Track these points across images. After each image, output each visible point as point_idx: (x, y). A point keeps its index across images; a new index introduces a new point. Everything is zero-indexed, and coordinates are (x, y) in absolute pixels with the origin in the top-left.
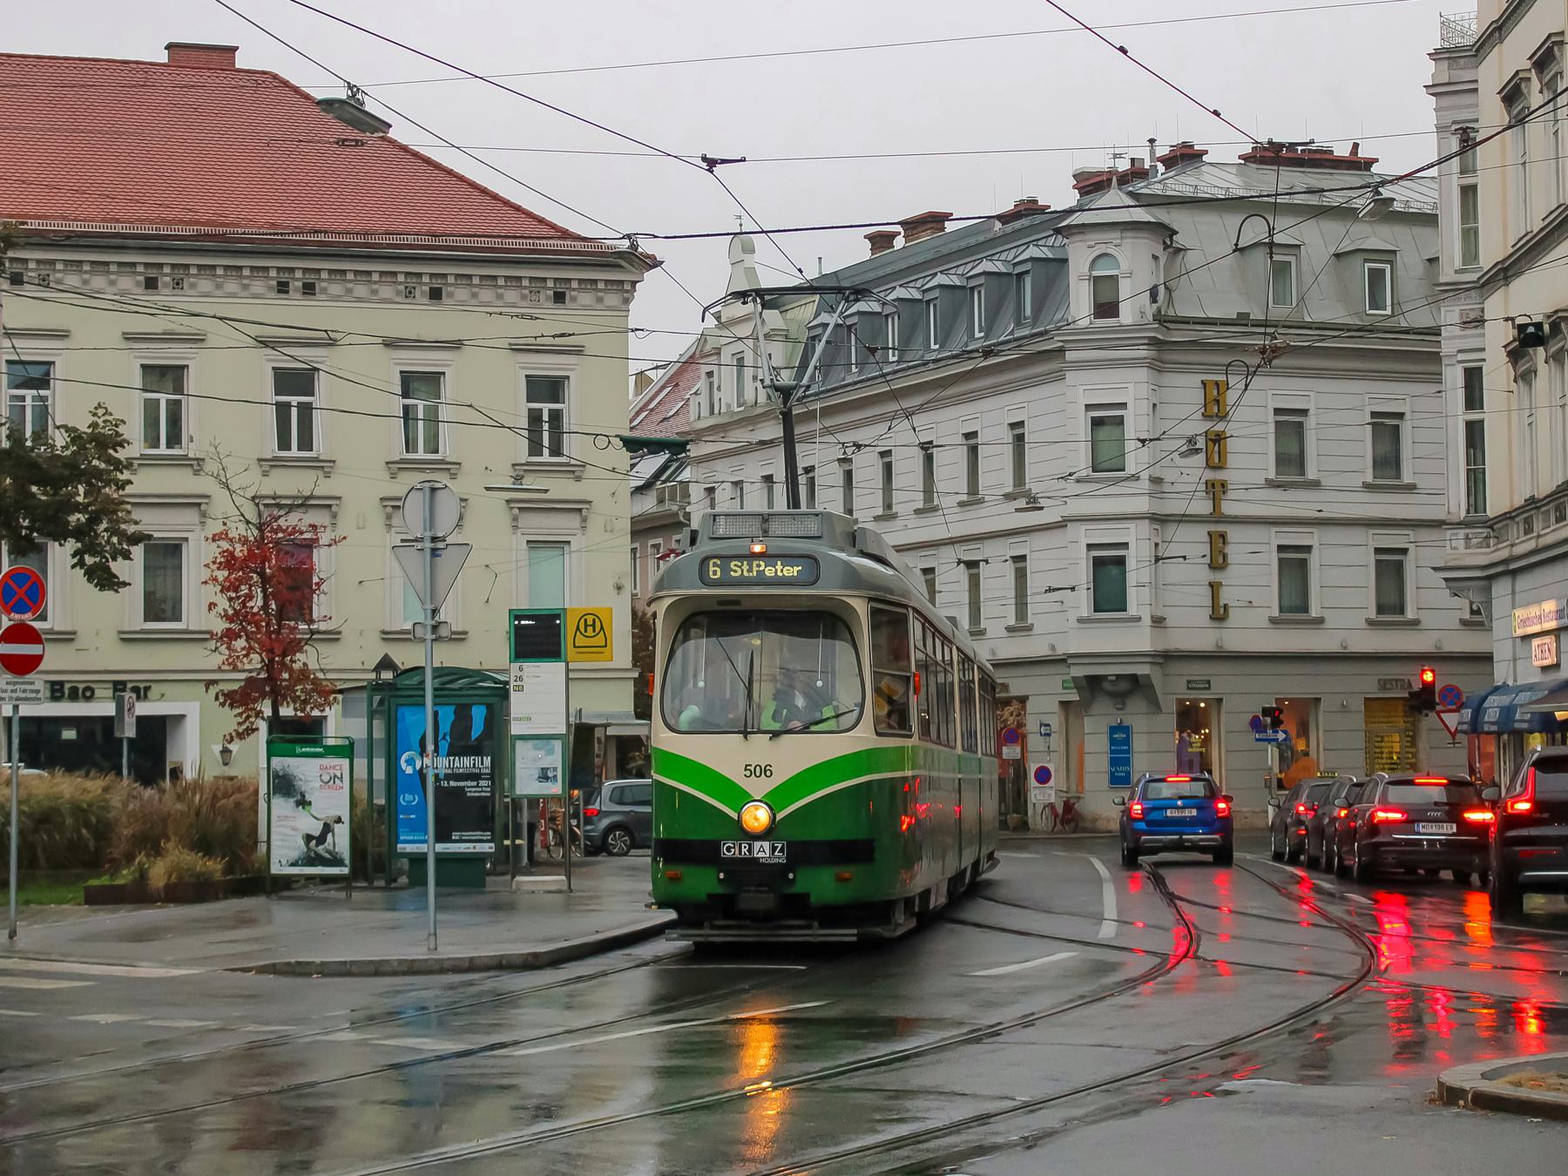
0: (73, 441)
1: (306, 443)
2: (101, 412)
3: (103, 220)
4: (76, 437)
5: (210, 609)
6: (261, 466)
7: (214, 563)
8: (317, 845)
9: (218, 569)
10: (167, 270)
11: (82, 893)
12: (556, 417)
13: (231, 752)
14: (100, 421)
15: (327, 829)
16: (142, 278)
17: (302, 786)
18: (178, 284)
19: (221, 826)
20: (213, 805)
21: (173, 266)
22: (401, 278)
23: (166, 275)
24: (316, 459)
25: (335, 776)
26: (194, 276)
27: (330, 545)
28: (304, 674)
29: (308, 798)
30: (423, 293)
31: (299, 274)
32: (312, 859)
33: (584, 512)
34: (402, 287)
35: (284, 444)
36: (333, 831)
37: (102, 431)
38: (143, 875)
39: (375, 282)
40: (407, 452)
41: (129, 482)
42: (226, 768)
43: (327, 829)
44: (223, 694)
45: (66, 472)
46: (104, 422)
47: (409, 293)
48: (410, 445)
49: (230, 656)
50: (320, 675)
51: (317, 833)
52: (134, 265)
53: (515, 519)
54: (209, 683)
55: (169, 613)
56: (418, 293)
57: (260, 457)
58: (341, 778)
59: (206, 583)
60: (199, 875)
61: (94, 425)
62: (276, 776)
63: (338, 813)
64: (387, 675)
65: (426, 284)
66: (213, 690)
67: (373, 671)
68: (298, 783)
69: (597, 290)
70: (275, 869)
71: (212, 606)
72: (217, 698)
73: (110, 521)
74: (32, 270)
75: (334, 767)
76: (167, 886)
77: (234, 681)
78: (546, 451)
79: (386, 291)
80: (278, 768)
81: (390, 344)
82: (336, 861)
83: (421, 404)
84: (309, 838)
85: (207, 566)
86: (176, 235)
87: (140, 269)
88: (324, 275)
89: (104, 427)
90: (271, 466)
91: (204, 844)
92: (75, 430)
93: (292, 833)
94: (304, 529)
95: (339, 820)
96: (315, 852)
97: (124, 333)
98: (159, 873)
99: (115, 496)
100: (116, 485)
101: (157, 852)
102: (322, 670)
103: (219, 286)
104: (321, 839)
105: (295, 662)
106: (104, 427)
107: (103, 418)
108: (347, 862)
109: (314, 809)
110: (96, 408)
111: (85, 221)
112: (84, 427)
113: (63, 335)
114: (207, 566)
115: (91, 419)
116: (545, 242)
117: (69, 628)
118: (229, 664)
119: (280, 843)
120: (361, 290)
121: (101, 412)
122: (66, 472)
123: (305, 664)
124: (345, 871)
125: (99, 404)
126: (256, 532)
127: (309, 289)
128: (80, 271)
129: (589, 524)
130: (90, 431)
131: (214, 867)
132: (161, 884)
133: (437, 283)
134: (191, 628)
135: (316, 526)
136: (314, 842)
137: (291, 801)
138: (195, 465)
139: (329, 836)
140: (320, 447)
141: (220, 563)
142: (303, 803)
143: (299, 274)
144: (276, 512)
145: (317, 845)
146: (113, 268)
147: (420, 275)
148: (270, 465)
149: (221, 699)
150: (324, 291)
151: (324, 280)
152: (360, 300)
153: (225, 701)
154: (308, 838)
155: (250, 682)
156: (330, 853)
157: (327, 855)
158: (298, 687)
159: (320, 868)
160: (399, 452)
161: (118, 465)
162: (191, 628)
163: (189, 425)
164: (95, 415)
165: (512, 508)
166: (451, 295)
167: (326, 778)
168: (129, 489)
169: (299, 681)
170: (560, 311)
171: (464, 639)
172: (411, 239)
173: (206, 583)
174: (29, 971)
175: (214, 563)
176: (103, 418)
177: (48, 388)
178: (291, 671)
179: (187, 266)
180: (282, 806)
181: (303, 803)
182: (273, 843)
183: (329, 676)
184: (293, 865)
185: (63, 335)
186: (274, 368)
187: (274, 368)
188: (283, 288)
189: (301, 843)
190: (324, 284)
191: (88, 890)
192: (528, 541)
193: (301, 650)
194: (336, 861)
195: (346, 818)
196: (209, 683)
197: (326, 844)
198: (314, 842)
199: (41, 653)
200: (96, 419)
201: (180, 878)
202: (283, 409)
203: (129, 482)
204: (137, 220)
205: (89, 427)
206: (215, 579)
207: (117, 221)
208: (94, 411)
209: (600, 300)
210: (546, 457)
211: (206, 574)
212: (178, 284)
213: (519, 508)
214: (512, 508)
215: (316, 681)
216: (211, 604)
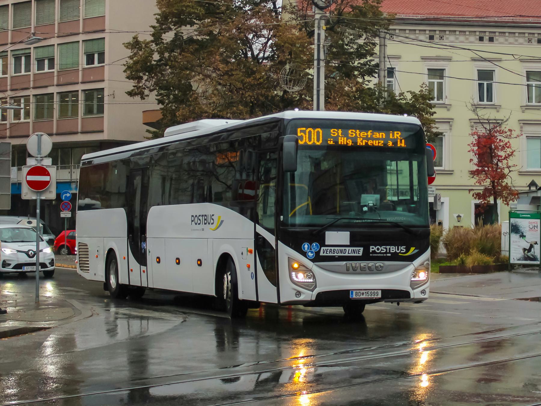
0: (413, 97)
1: (490, 99)
2: (424, 86)
3: (413, 14)
4: (414, 96)
5: (470, 162)
6: (522, 109)
7: (472, 144)
8: (528, 253)
9: (473, 146)
10: (437, 32)
11: (439, 268)
12: (440, 85)
13: (461, 217)
14: (424, 90)
15: (531, 246)
16: (478, 37)
17: (522, 229)
18: (441, 38)
19: (489, 245)
20: (486, 236)
21: (440, 31)
22: (527, 35)
23: (437, 34)
24: (494, 105)
25: (535, 226)
26: (448, 34)
27: (516, 137)
28: (506, 187)
29: (524, 234)
30: (535, 41)
31: (487, 34)
32: (527, 258)
33: (451, 123)
34: (527, 39)
35: (481, 99)
36: (534, 247)
37: (425, 93)
38: (463, 262)
39: (507, 36)
40: (529, 102)
41: (435, 113)
42: (459, 223)
43: (531, 246)
44: (476, 194)
45: (412, 109)
46: (425, 90)
47: (530, 41)
48: (529, 99)
49: (479, 180)
50: (513, 189)
51: (528, 248)
52: (425, 30)
53: (521, 127)
54: (470, 190)
55: (437, 164)
56: (533, 41)
57: (521, 105)
58: (537, 227)
59: (469, 151)
60: (485, 263)
61: (422, 91)
62: (512, 225)
63: (536, 240)
64: (533, 188)
65: (536, 37)
66: (472, 193)
67: (528, 186)
68: (521, 229)
69: (515, 37)
70: (512, 261)
71: (471, 160)
72: (473, 196)
73: (427, 127)
74: (437, 34)
75: (534, 223)
76: (473, 267)
77: (480, 189)
78: (436, 99)
79: (521, 40)
80: (513, 223)
81: (424, 59)
82: (534, 259)
83: (485, 83)
84: (525, 250)
85: (469, 145)
86: (412, 19)
87: (478, 33)
88: (497, 34)
89: (425, 92)
90: (526, 109)
91: (483, 251)
92: (414, 93)
93: (518, 247)
94: (507, 131)
95: (536, 243)
96: (527, 255)
97: (421, 57)
98: (470, 261)
99: (429, 117)
100: (430, 114)
101: (468, 253)
102: (514, 187)
103: (457, 39)
104: (529, 250)
105: (503, 182)
106: (425, 92)
107: (425, 88)
108: (539, 259)
109: (526, 239)
110: (422, 85)
111: (406, 14)
112: (417, 92)
113: (449, 59)
114: (469, 145)
115: (420, 89)
116: (508, 18)
117: (451, 169)
118: (479, 183)
119: (514, 251)
120: (511, 40)
121: (424, 86)
122: (412, 109)
123: (507, 183)
124: (538, 263)
125: (423, 83)
126: (488, 132)
127: (491, 40)
128: (505, 36)
129: (453, 128)
130: (420, 93)
131: (489, 260)
132: (471, 266)
133: (492, 35)
134: (446, 169)
135: (511, 130)
136: (526, 251)
137: (518, 235)
138: (496, 108)
139: (532, 249)
140: (496, 100)
141: (475, 144)
142: (523, 236)
143: (487, 34)
144: (496, 125)
145: (528, 253)
146: (417, 32)
147: (534, 34)
148: (525, 108)
149: (475, 196)
150: (497, 40)
151: (497, 36)
152: (510, 43)
153: (476, 197)
154: (525, 250)
155: (486, 190)
156: (533, 256)
157: (532, 257)
158: (504, 192)
159: (529, 261)
160: (525, 102)
161: (431, 106)
162: (446, 169)
163: (446, 91)
164: (422, 87)
165: (471, 122)
166: (497, 40)
167: (531, 227)
168: (435, 116)
169: (504, 190)
170: (491, 44)
171: (452, 174)
172: (531, 20)
173: (469, 151)
174: (444, 298)
175: (472, 144)
176: (425, 88)
177: (443, 79)
178: (501, 186)
179: (445, 31)
180: (515, 237)
181: (523, 236)
182: (511, 251)
183: (517, 189)
184: (518, 260)
185: (449, 59)
186: (478, 70)
187: (478, 70)
188: (481, 39)
189: (522, 251)
190: (497, 38)
191: (440, 267)
192: (526, 136)
193: (505, 178)
194: (534, 259)
195: (539, 242)
196: (470, 190)
197: (531, 252)
198: (526, 251)
199: (28, 176)
200: (422, 89)
201: (479, 264)
202: (480, 85)
203: (435, 113)
204: (426, 14)
205: (419, 92)
206: (473, 150)
207: (419, 14)
208: (422, 86)
209: (467, 39)
210: (485, 102)
211: (469, 148)
212: (441, 38)
213: (523, 123)
214: (471, 122)
215: (510, 190)
216: (471, 159)
